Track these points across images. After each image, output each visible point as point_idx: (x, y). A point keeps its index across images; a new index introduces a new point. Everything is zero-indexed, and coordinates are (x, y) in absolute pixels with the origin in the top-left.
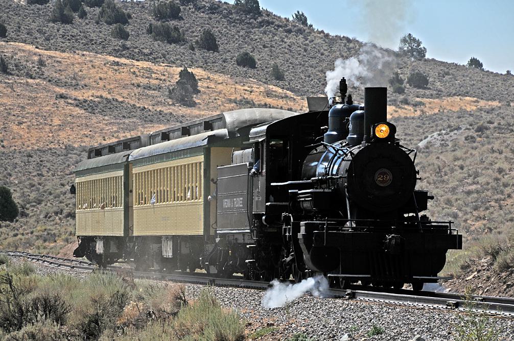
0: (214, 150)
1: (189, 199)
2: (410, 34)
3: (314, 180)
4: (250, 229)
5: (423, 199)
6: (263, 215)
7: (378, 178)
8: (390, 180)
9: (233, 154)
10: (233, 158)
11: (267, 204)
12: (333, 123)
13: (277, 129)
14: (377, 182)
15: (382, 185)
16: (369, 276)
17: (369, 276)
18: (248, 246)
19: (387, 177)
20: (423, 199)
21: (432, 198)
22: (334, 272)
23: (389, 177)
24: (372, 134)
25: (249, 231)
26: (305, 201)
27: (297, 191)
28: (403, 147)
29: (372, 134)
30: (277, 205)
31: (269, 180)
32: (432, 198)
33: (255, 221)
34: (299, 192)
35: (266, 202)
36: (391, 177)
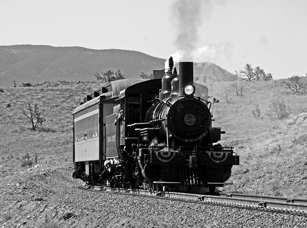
0: (105, 105)
1: (96, 137)
2: (248, 66)
3: (152, 122)
4: (118, 156)
5: (217, 133)
6: (124, 146)
7: (187, 120)
8: (195, 121)
9: (113, 108)
10: (113, 110)
11: (126, 138)
12: (164, 86)
13: (131, 91)
14: (186, 123)
15: (189, 125)
16: (179, 183)
17: (179, 183)
18: (117, 166)
19: (192, 119)
20: (217, 133)
21: (224, 132)
22: (158, 181)
23: (194, 119)
24: (197, 98)
25: (118, 157)
26: (144, 135)
27: (140, 129)
28: (203, 100)
29: (197, 98)
30: (131, 139)
31: (126, 124)
32: (224, 132)
33: (120, 150)
34: (141, 130)
35: (125, 138)
36: (195, 119)
